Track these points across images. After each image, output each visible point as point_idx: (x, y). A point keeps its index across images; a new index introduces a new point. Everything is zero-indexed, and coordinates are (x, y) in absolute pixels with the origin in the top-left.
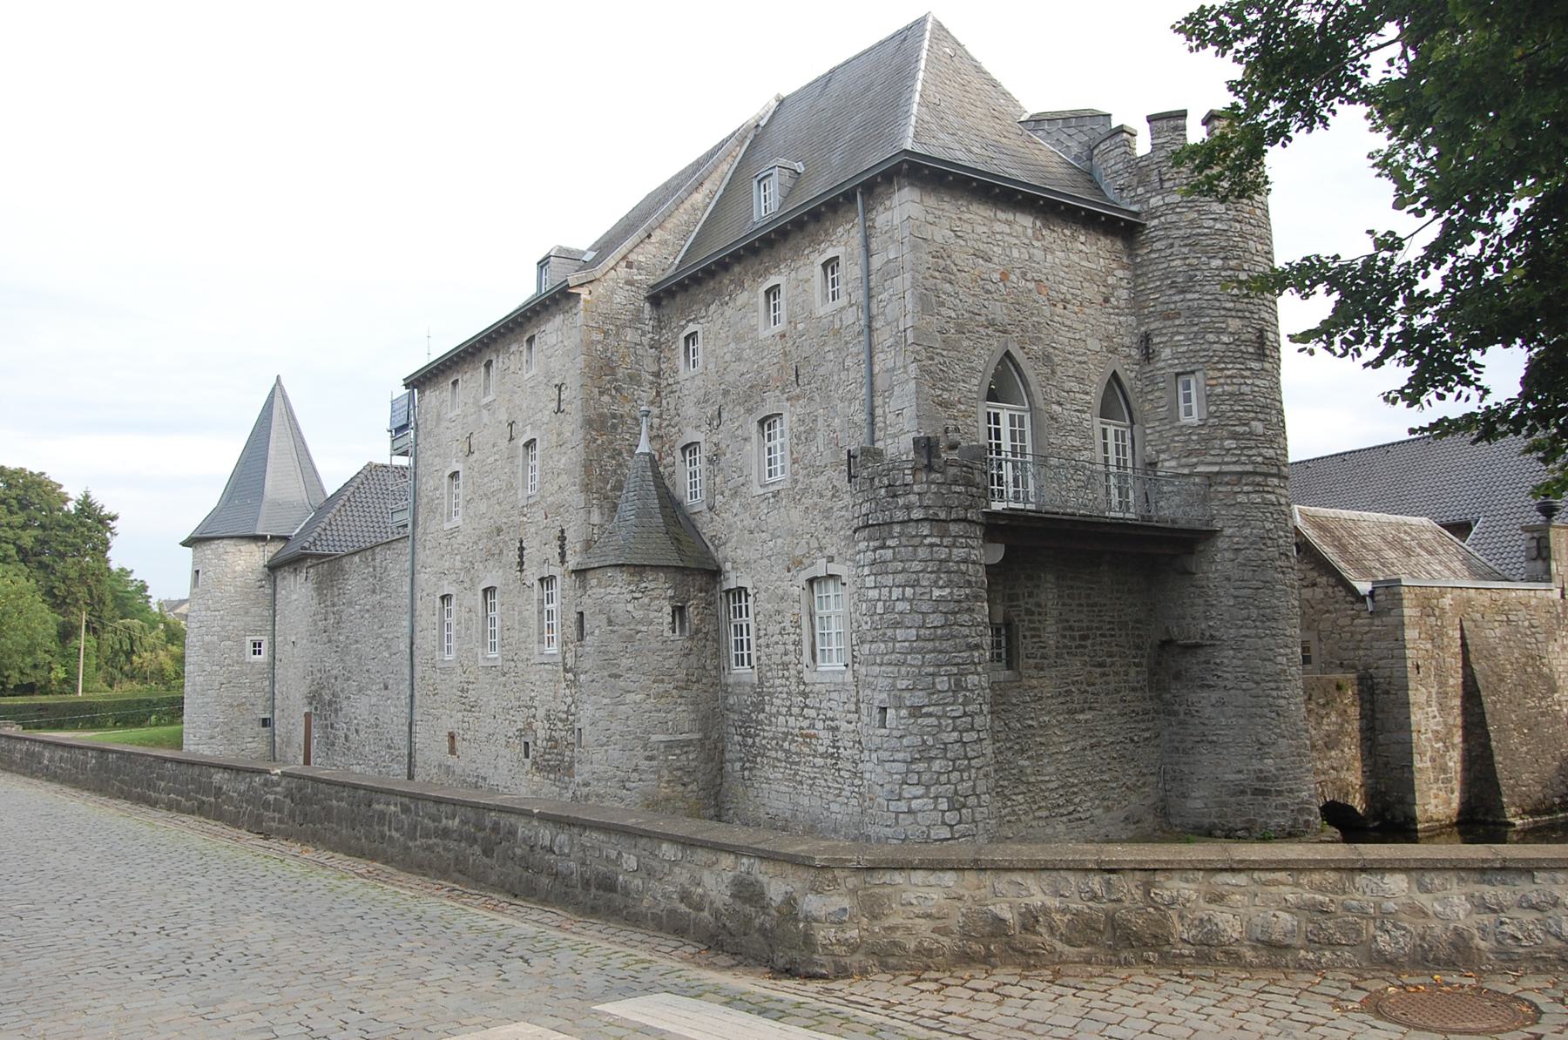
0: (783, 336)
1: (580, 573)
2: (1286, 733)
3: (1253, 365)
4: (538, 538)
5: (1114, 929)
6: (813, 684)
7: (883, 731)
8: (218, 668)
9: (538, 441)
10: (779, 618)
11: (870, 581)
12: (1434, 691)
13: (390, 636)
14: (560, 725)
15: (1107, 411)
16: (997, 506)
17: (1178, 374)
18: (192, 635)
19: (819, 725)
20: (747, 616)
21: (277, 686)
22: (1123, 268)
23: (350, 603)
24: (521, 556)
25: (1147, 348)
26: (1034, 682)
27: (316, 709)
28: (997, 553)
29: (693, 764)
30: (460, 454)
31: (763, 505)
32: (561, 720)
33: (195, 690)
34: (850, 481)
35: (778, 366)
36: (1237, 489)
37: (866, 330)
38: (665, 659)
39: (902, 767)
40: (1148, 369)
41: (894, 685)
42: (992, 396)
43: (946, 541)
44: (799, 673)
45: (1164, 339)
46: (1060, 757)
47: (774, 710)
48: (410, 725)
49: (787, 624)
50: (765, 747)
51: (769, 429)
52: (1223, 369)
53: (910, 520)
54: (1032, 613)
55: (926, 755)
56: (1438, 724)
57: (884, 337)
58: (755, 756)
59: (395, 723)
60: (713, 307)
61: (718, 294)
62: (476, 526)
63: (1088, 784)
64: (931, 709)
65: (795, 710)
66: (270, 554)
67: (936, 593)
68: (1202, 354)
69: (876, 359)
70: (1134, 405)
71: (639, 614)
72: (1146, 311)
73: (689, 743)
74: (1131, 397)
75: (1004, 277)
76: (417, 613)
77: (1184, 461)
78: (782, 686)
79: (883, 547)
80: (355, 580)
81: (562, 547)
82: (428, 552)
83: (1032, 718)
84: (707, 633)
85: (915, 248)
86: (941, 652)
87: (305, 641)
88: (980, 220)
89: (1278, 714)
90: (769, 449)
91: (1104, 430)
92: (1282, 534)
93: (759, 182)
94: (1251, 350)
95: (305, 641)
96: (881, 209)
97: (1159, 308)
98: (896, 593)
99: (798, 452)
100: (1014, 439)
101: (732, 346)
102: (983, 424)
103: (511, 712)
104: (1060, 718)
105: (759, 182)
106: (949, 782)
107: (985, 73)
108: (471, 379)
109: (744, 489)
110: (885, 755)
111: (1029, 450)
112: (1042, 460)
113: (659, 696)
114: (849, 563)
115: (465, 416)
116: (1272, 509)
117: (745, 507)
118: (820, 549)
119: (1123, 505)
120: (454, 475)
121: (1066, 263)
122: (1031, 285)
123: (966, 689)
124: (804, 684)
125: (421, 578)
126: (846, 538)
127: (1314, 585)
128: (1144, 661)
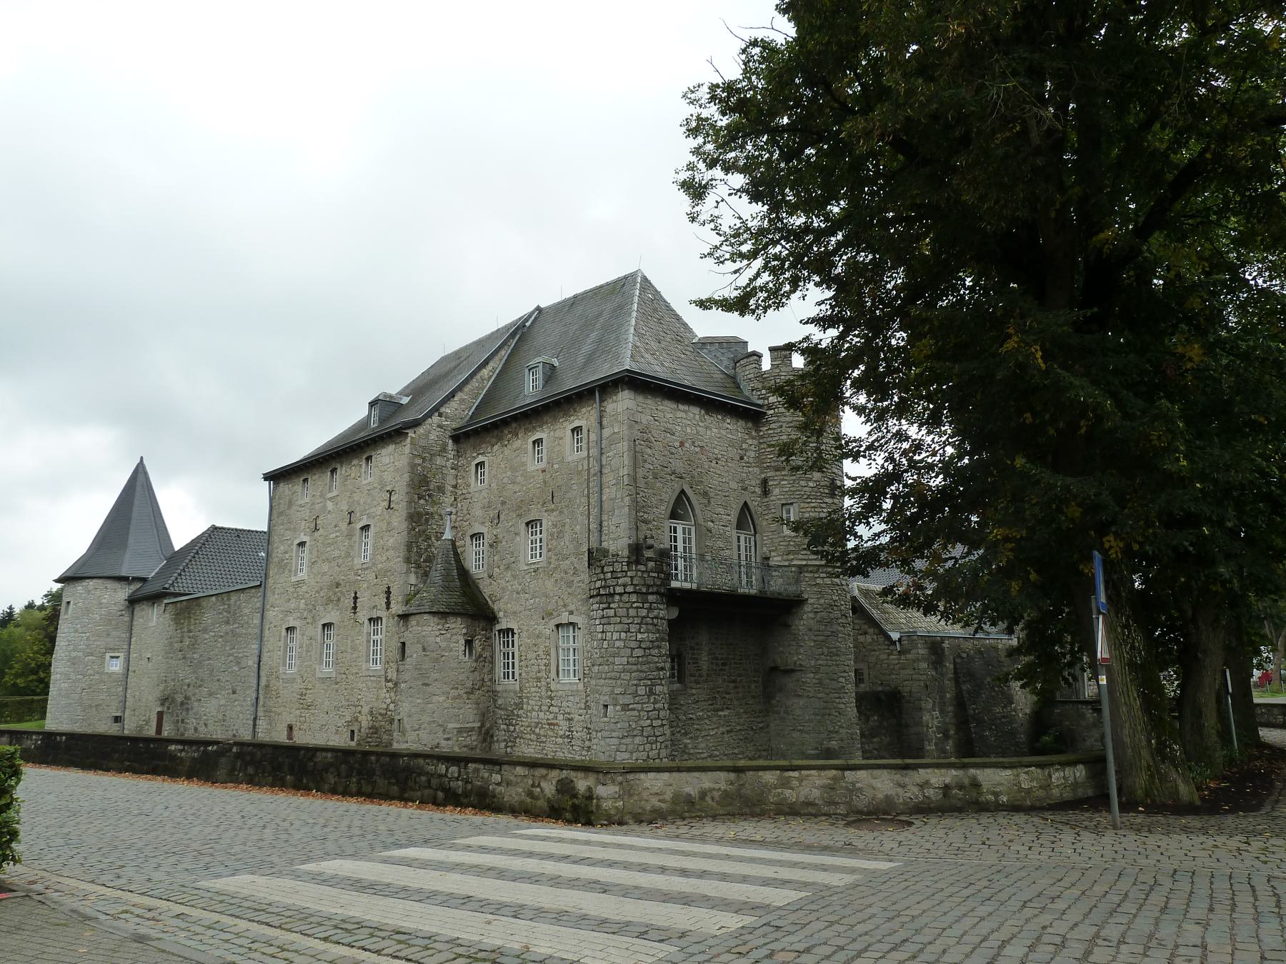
0: (544, 471)
1: (404, 617)
2: (844, 725)
3: (827, 500)
4: (370, 591)
5: (740, 798)
6: (557, 691)
7: (605, 719)
8: (81, 677)
9: (372, 527)
10: (535, 649)
11: (600, 628)
12: (937, 701)
13: (240, 655)
14: (380, 718)
15: (741, 525)
16: (674, 584)
17: (783, 505)
18: (61, 651)
19: (561, 717)
20: (513, 646)
21: (129, 691)
22: (753, 438)
23: (205, 631)
24: (355, 603)
25: (765, 487)
26: (694, 691)
27: (168, 708)
28: (674, 613)
29: (475, 743)
30: (308, 530)
31: (527, 576)
32: (380, 714)
33: (60, 694)
34: (589, 567)
35: (540, 490)
36: (816, 575)
37: (599, 474)
38: (459, 674)
39: (615, 741)
40: (766, 500)
41: (613, 691)
42: (674, 515)
43: (646, 605)
44: (548, 684)
45: (776, 483)
46: (709, 738)
47: (530, 708)
48: (255, 719)
49: (540, 653)
50: (522, 732)
51: (532, 528)
52: (809, 503)
53: (625, 593)
54: (694, 649)
55: (630, 733)
56: (940, 722)
57: (609, 478)
58: (516, 738)
59: (241, 718)
60: (496, 447)
61: (500, 439)
62: (318, 580)
63: (726, 755)
64: (635, 706)
65: (544, 708)
66: (131, 591)
67: (639, 636)
68: (798, 493)
69: (604, 492)
70: (756, 522)
71: (444, 645)
72: (765, 465)
73: (472, 729)
74: (755, 517)
75: (682, 444)
76: (265, 639)
77: (785, 557)
78: (535, 692)
79: (609, 608)
80: (209, 616)
81: (388, 598)
82: (276, 596)
83: (692, 714)
84: (485, 658)
85: (630, 427)
86: (641, 671)
87: (160, 658)
88: (667, 411)
89: (840, 713)
90: (532, 541)
91: (739, 537)
92: (843, 603)
93: (529, 370)
94: (826, 491)
95: (160, 658)
96: (610, 401)
97: (773, 464)
98: (616, 636)
99: (552, 545)
100: (685, 542)
101: (509, 473)
102: (667, 534)
103: (342, 709)
104: (709, 714)
105: (529, 370)
106: (644, 750)
107: (673, 310)
108: (319, 481)
109: (514, 565)
110: (606, 734)
111: (694, 551)
112: (701, 557)
113: (454, 698)
114: (583, 616)
115: (313, 504)
116: (837, 588)
117: (514, 577)
118: (565, 606)
119: (749, 583)
120: (302, 544)
121: (719, 435)
122: (697, 449)
123: (655, 694)
124: (551, 691)
125: (270, 614)
126: (582, 600)
127: (866, 633)
128: (760, 680)
